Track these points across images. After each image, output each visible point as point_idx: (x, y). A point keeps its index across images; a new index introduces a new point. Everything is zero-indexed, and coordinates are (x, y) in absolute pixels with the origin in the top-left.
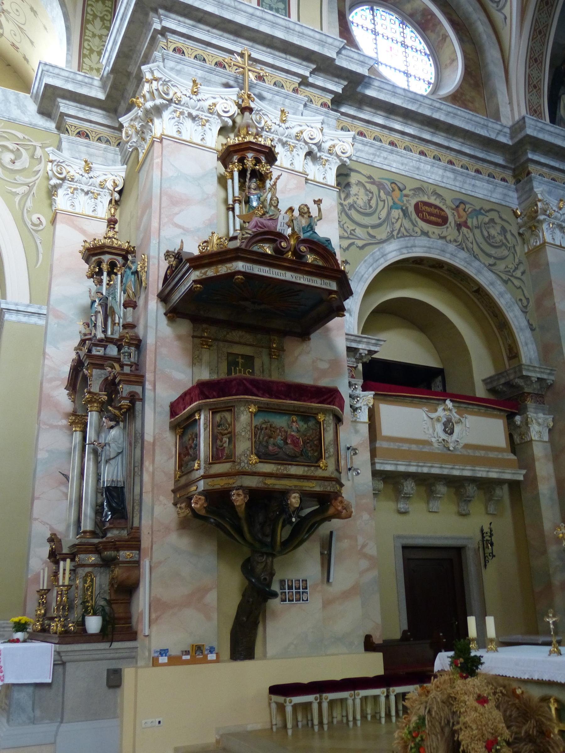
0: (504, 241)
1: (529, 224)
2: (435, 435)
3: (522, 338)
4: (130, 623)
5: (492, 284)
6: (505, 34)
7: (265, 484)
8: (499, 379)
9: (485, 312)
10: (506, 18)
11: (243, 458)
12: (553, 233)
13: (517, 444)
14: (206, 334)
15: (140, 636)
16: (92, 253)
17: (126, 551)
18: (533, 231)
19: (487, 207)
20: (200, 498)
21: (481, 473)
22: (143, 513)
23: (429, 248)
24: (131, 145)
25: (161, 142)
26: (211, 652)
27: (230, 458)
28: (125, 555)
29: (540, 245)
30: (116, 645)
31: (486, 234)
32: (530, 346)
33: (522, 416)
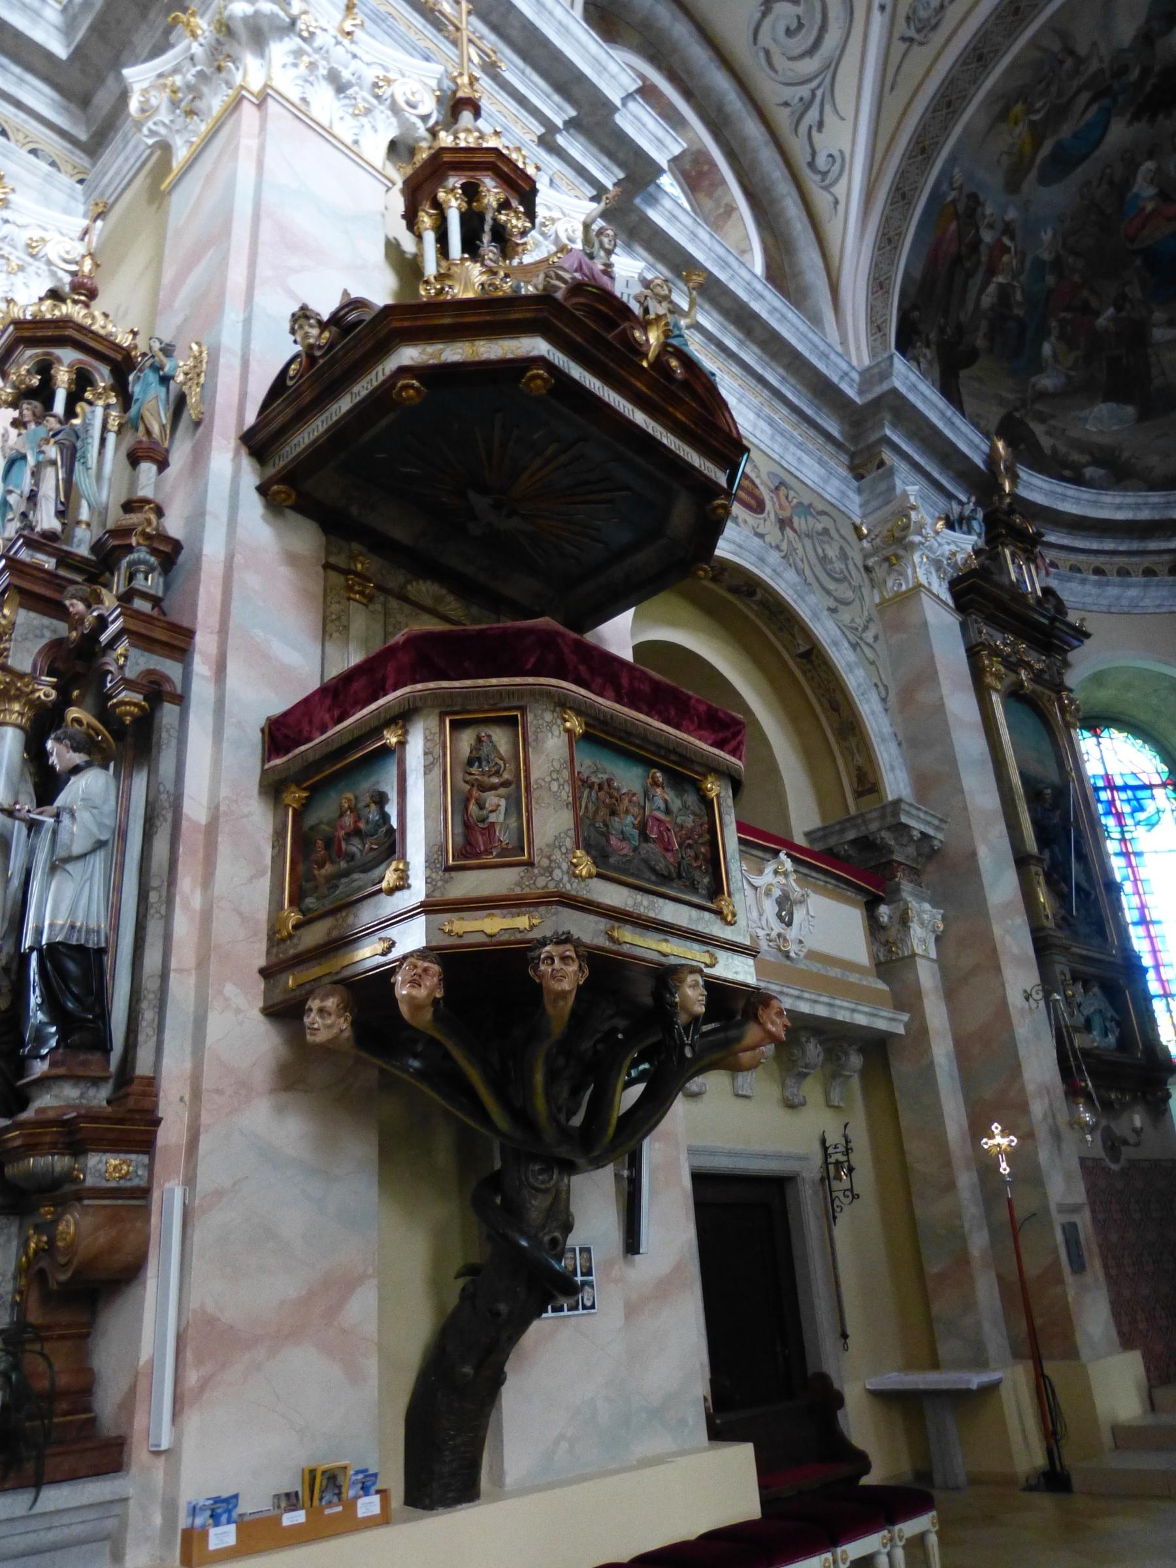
0: (846, 573)
1: (886, 553)
2: (764, 923)
3: (885, 755)
4: (88, 1409)
5: (835, 644)
6: (833, 231)
7: (612, 939)
8: (842, 831)
9: (814, 701)
10: (836, 202)
11: (557, 856)
12: (928, 573)
13: (891, 961)
14: (359, 566)
15: (139, 1455)
16: (27, 334)
17: (105, 1157)
18: (891, 565)
19: (820, 506)
20: (425, 970)
21: (842, 1012)
22: (168, 1036)
23: (740, 546)
24: (154, 128)
25: (261, 105)
26: (366, 1490)
27: (517, 853)
28: (104, 1167)
29: (909, 590)
30: (55, 1497)
31: (820, 551)
32: (898, 772)
33: (894, 905)
